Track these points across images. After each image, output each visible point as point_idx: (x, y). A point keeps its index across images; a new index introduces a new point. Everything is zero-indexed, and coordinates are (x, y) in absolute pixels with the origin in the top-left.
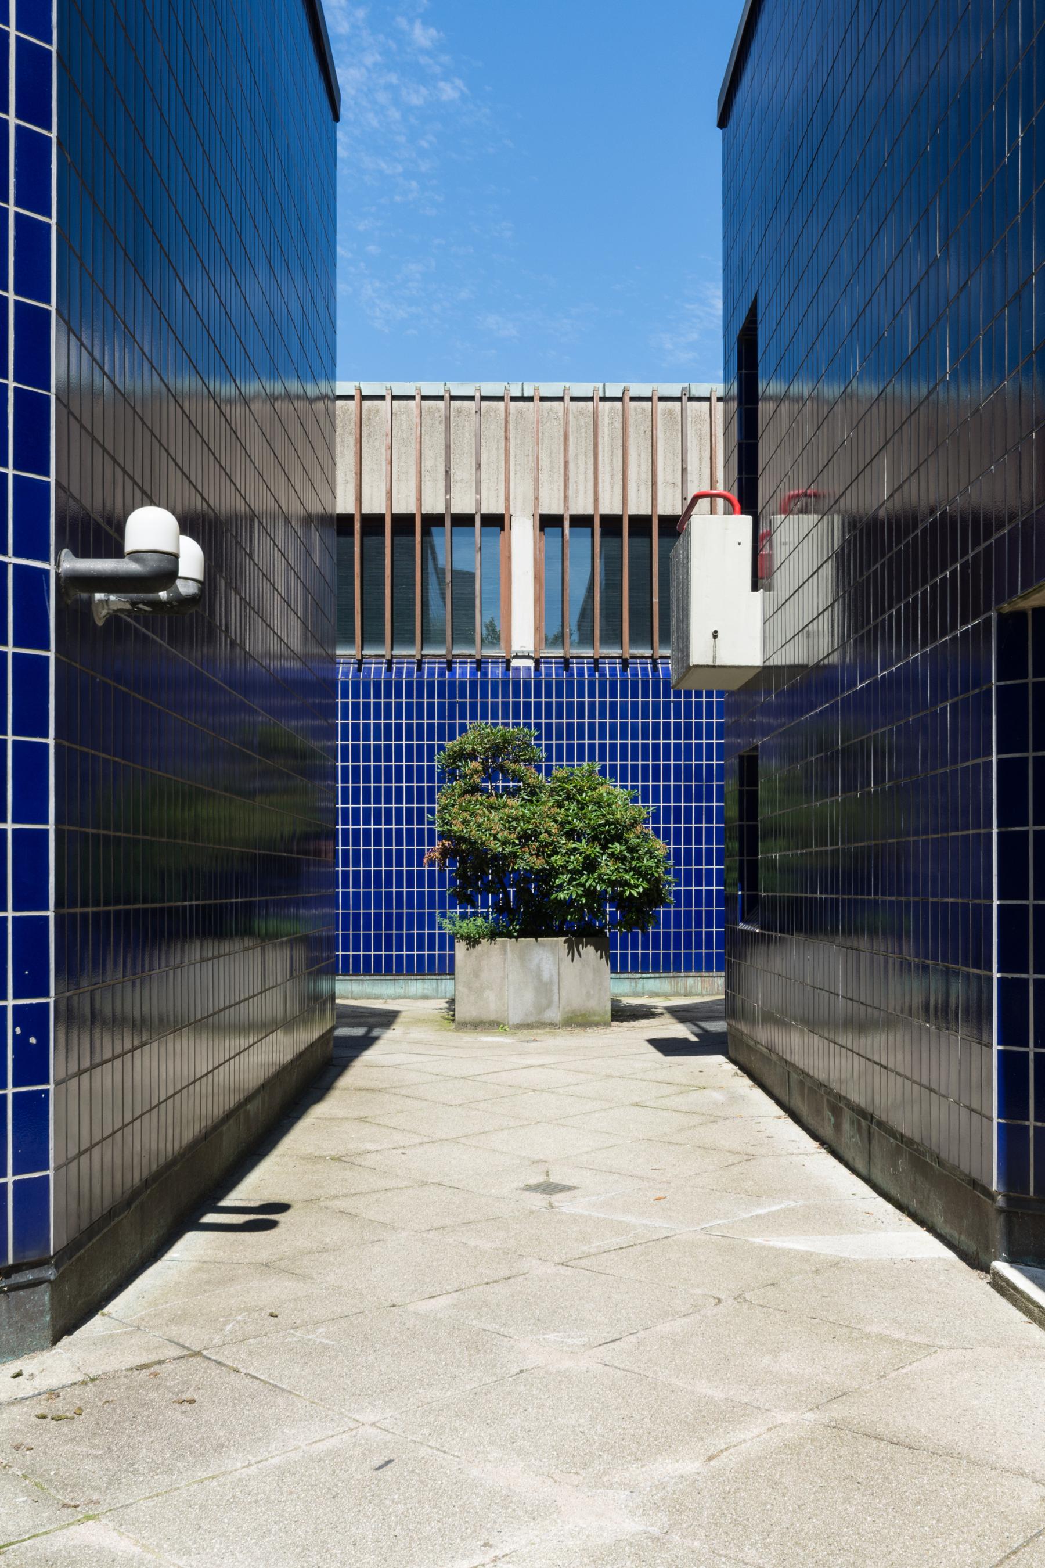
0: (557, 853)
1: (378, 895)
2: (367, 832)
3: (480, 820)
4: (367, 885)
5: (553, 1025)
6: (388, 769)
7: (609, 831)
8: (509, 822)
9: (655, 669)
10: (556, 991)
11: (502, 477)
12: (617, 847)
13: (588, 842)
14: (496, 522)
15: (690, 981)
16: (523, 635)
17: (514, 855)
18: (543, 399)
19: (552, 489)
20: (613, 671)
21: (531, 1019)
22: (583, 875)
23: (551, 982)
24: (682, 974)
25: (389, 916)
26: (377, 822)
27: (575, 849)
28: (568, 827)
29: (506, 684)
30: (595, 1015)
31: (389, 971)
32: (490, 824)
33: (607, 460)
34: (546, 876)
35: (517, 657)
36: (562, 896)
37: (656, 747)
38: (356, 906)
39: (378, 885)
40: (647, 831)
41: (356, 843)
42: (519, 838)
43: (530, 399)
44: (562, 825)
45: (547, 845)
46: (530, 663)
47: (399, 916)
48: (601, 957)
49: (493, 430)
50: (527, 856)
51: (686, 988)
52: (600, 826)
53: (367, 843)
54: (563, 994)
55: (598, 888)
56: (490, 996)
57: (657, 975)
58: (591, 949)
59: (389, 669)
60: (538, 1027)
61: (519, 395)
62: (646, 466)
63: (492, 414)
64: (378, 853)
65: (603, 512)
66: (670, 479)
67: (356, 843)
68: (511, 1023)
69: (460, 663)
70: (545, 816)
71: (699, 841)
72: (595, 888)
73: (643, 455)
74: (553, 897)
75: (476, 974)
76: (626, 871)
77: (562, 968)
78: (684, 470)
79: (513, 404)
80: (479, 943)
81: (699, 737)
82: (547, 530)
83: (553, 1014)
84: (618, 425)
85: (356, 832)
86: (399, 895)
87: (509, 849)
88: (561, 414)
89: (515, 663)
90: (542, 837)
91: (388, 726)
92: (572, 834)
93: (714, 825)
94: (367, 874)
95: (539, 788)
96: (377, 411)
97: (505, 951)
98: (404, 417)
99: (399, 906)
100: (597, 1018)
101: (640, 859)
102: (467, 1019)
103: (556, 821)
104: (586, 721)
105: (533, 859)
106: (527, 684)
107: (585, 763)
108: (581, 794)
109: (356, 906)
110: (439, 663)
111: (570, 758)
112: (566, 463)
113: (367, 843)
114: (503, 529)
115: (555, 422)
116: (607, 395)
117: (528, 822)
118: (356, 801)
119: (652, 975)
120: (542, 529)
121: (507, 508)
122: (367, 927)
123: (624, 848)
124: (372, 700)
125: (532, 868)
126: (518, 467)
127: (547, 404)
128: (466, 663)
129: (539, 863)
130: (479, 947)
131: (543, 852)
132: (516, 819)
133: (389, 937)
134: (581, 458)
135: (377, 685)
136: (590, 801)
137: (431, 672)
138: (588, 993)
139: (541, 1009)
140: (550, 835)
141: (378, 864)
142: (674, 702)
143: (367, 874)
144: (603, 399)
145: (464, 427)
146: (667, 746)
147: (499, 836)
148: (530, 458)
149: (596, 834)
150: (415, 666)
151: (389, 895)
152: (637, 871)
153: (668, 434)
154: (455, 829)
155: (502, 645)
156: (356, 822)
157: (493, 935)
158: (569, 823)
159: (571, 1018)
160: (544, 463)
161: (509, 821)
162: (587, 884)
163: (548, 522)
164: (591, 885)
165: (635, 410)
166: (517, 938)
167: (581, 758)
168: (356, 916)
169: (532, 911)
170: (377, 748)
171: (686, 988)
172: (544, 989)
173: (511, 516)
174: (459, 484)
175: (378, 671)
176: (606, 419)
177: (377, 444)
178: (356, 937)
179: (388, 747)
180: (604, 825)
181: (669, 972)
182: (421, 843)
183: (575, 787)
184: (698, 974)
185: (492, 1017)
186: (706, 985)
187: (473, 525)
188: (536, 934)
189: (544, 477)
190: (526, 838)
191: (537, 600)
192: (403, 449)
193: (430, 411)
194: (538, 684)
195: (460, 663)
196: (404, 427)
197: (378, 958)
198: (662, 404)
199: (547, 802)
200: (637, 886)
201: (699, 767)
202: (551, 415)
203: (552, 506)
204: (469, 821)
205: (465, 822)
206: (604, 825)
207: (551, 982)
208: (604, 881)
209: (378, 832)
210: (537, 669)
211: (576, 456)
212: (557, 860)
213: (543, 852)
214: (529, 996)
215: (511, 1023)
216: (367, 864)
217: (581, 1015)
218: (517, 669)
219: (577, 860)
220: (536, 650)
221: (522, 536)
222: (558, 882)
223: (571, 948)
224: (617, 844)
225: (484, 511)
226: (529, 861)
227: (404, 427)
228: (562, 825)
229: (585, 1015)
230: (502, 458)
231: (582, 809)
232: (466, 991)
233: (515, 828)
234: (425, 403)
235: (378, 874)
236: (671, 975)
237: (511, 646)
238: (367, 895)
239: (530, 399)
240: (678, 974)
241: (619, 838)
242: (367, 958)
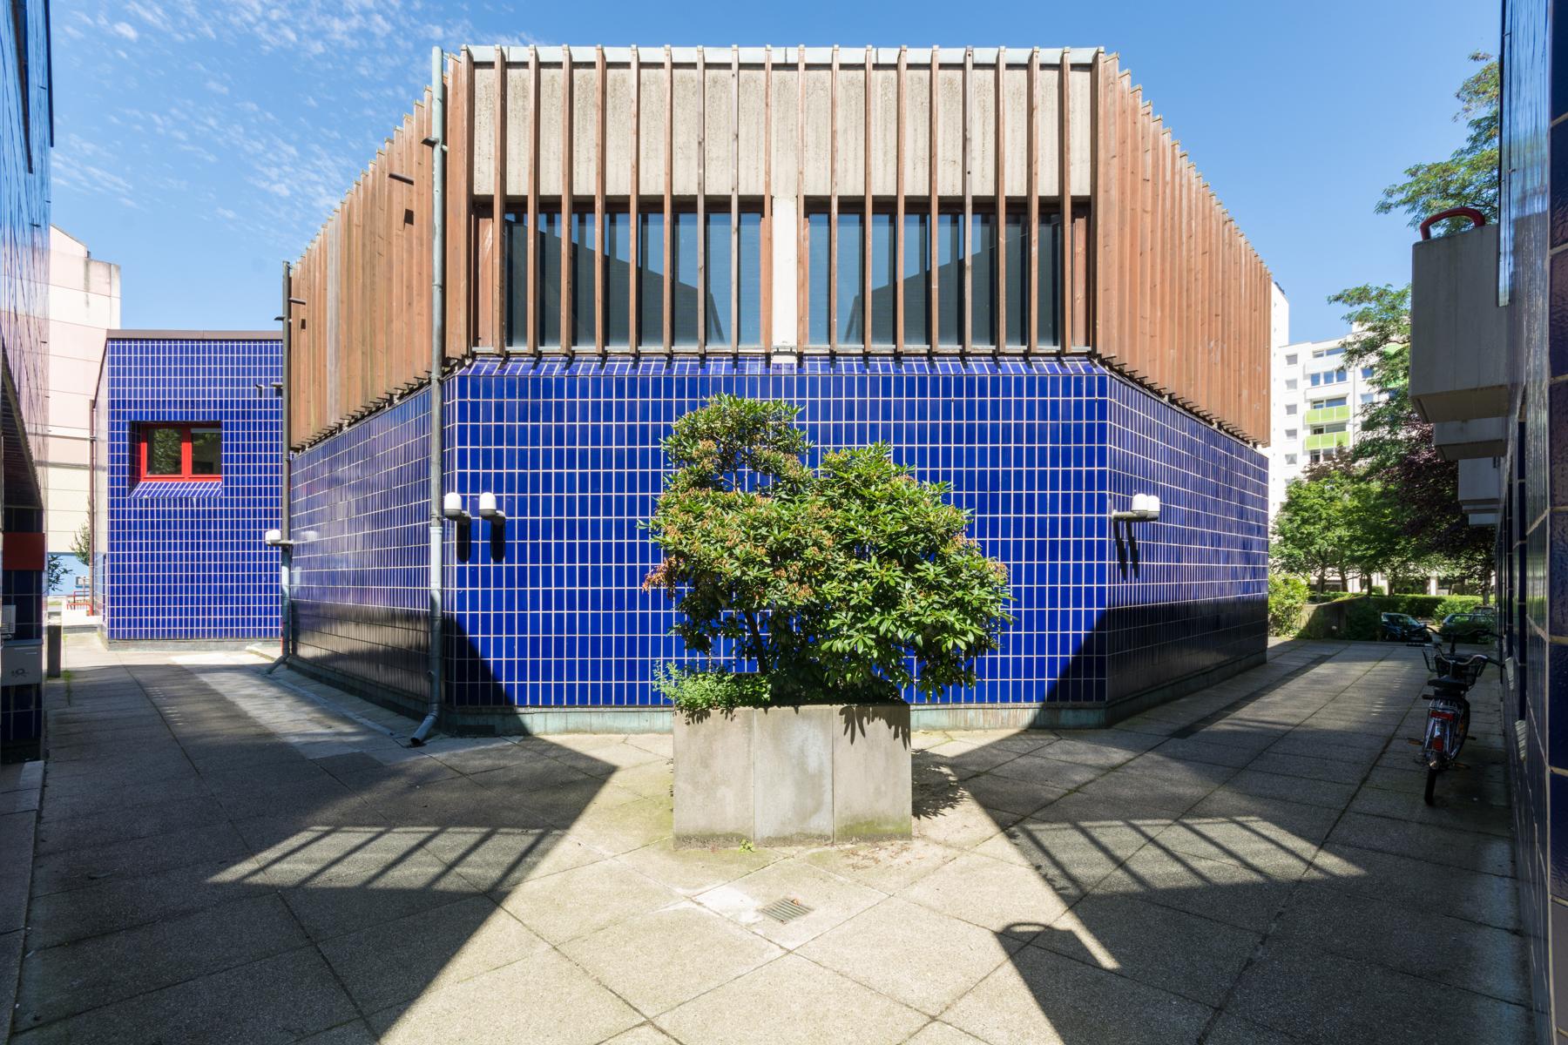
0: (832, 578)
1: (620, 617)
2: (608, 547)
4: (608, 606)
5: (822, 838)
6: (632, 476)
8: (755, 528)
9: (932, 366)
11: (762, 154)
12: (930, 570)
14: (754, 206)
15: (971, 713)
16: (784, 325)
18: (809, 67)
21: (790, 830)
22: (872, 612)
25: (632, 641)
26: (620, 535)
28: (851, 537)
29: (765, 380)
31: (631, 702)
32: (725, 532)
34: (818, 611)
35: (778, 353)
36: (839, 645)
39: (620, 606)
41: (595, 559)
42: (772, 553)
43: (794, 67)
44: (841, 534)
46: (793, 360)
47: (644, 641)
48: (896, 736)
49: (753, 102)
50: (783, 583)
53: (608, 559)
54: (839, 791)
56: (728, 795)
58: (881, 724)
59: (635, 366)
60: (800, 842)
64: (620, 570)
67: (595, 559)
68: (758, 836)
71: (595, 536)
72: (894, 635)
73: (920, 130)
75: (705, 763)
79: (775, 73)
80: (708, 714)
81: (983, 440)
83: (823, 822)
85: (596, 547)
86: (644, 617)
87: (753, 573)
89: (775, 360)
91: (632, 429)
92: (856, 549)
94: (608, 594)
95: (803, 484)
96: (624, 81)
97: (750, 727)
99: (644, 630)
100: (890, 828)
102: (691, 832)
103: (829, 528)
106: (789, 381)
107: (868, 445)
108: (868, 487)
109: (596, 630)
112: (833, 133)
113: (608, 559)
116: (881, 61)
118: (595, 512)
120: (806, 215)
121: (768, 185)
123: (939, 569)
125: (791, 604)
129: (803, 595)
130: (707, 722)
131: (810, 578)
132: (768, 524)
133: (632, 664)
135: (620, 383)
136: (881, 498)
137: (682, 368)
139: (804, 815)
140: (821, 549)
141: (620, 582)
143: (608, 594)
144: (877, 66)
146: (947, 451)
147: (737, 551)
151: (632, 617)
154: (668, 539)
156: (595, 536)
157: (730, 703)
158: (852, 531)
159: (851, 827)
160: (810, 138)
161: (756, 529)
162: (882, 629)
163: (815, 206)
164: (888, 630)
166: (766, 705)
168: (596, 641)
169: (789, 665)
170: (620, 453)
172: (809, 783)
177: (623, 117)
179: (632, 452)
180: (907, 534)
183: (858, 476)
185: (730, 827)
186: (989, 717)
190: (781, 555)
191: (800, 287)
192: (652, 123)
193: (683, 81)
194: (801, 381)
197: (620, 688)
200: (964, 633)
201: (982, 474)
203: (819, 189)
205: (685, 529)
206: (907, 534)
208: (909, 625)
209: (620, 547)
210: (800, 365)
211: (845, 131)
212: (832, 589)
213: (810, 578)
214: (786, 795)
215: (758, 836)
216: (608, 583)
218: (778, 367)
219: (864, 589)
221: (785, 222)
222: (833, 623)
223: (849, 721)
224: (928, 564)
226: (788, 592)
230: (763, 133)
231: (871, 508)
233: (764, 538)
235: (620, 594)
239: (794, 67)
241: (932, 554)
242: (607, 688)
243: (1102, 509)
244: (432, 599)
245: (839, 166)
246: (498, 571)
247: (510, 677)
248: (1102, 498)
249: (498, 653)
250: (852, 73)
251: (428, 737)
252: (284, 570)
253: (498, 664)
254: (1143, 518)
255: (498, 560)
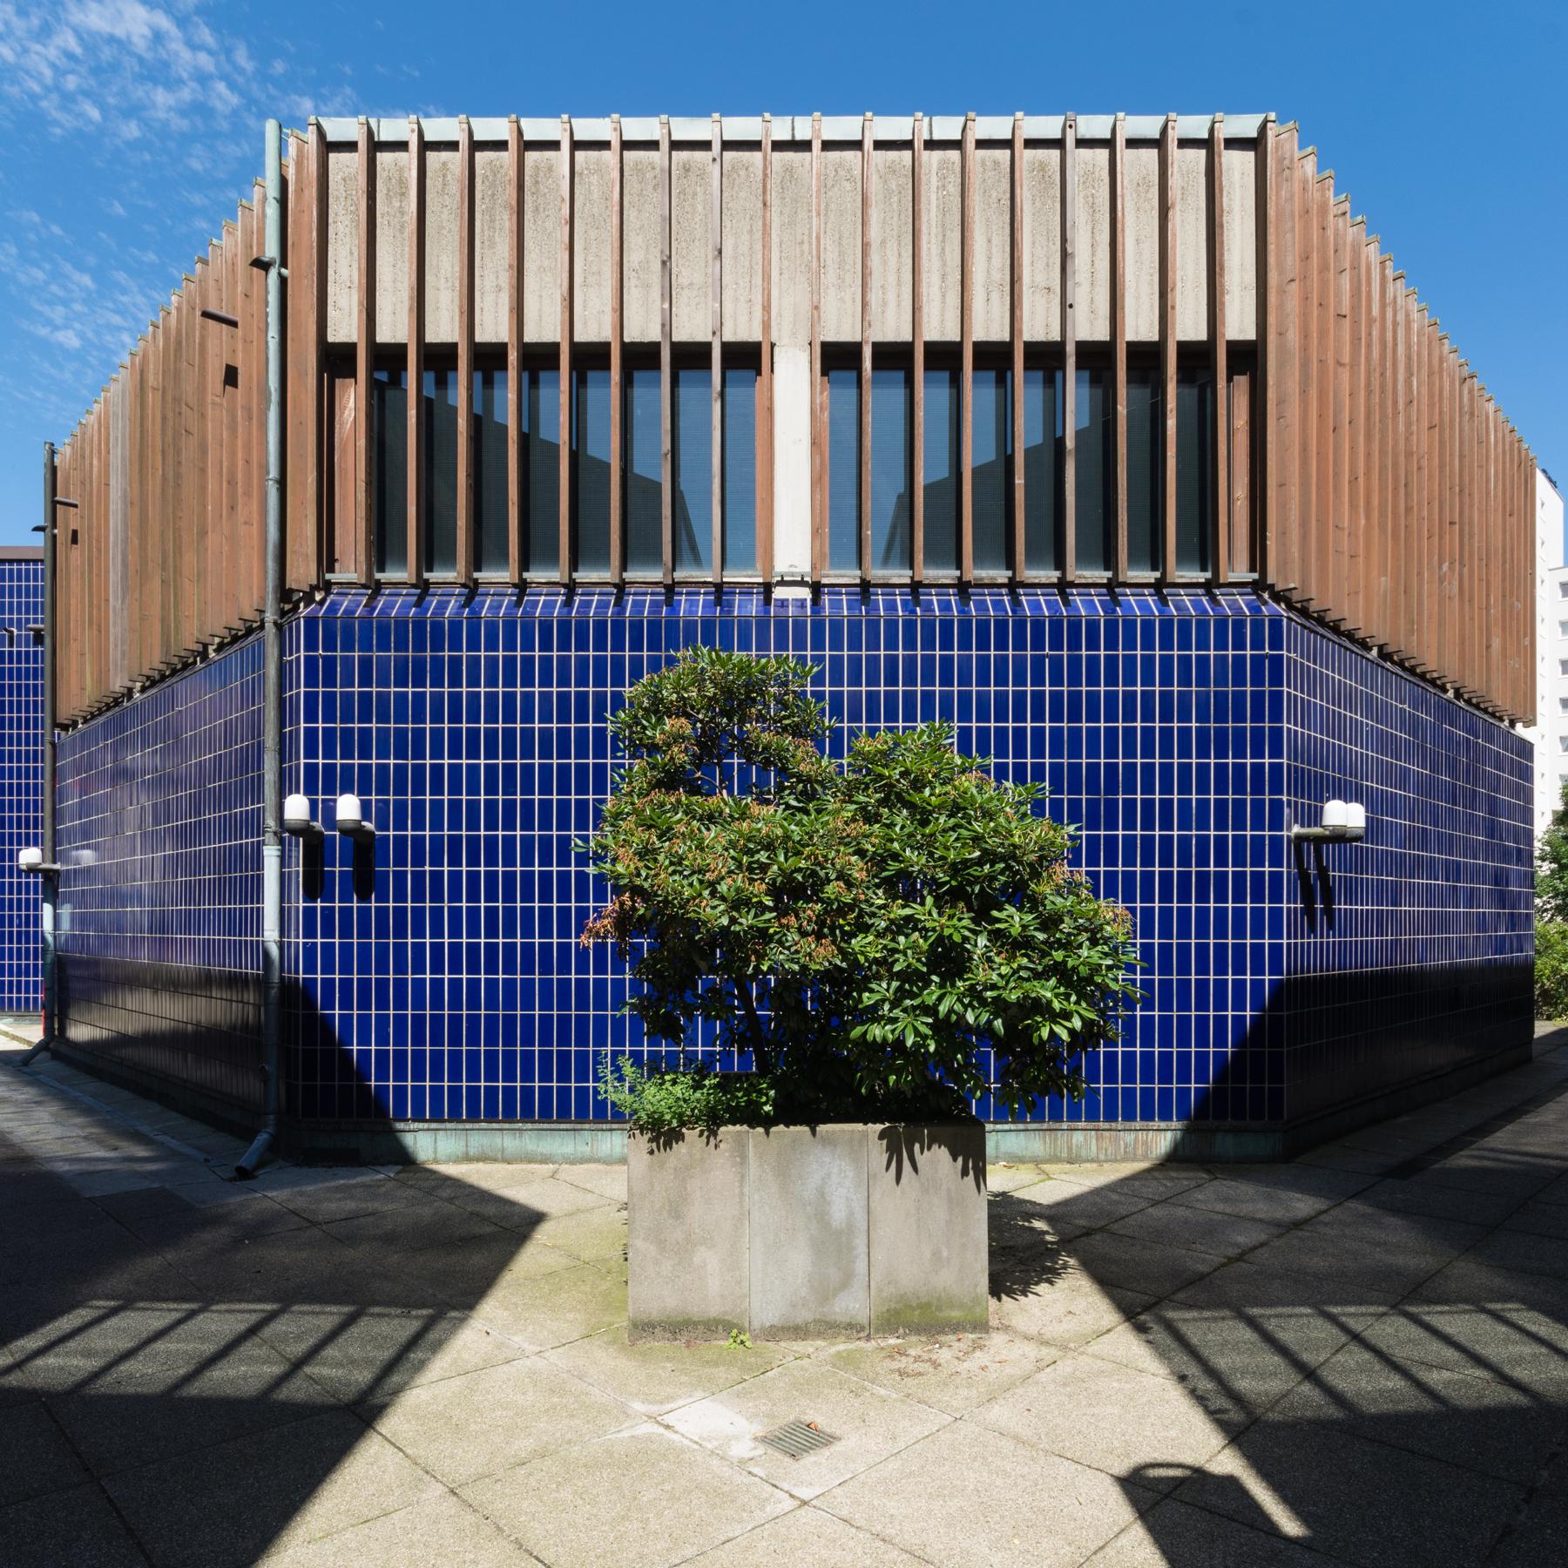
0: (866, 929)
3: (681, 849)
5: (853, 1329)
7: (992, 878)
8: (751, 853)
9: (1016, 603)
10: (862, 1249)
11: (758, 280)
12: (1014, 919)
13: (938, 905)
14: (746, 359)
15: (1078, 1137)
16: (793, 542)
17: (763, 935)
19: (842, 300)
20: (945, 606)
21: (804, 1316)
22: (928, 983)
23: (850, 1228)
24: (1065, 1125)
27: (908, 919)
28: (894, 866)
29: (763, 624)
30: (952, 1306)
31: (564, 1115)
32: (707, 857)
33: (935, 250)
35: (782, 583)
36: (876, 1032)
37: (1020, 733)
38: (510, 1004)
40: (1077, 877)
41: (509, 896)
42: (775, 891)
43: (805, 146)
44: (878, 861)
45: (844, 909)
46: (805, 593)
48: (965, 1173)
50: (792, 936)
51: (1070, 1149)
52: (966, 863)
54: (879, 1256)
55: (970, 1017)
56: (709, 1260)
57: (1021, 1126)
58: (941, 1153)
60: (819, 1335)
61: (788, 137)
62: (1001, 259)
63: (742, 173)
65: (927, 338)
66: (1041, 279)
68: (756, 1324)
69: (688, 594)
70: (836, 835)
72: (962, 1017)
74: (857, 1032)
76: (1037, 976)
77: (876, 1196)
78: (1065, 255)
79: (777, 155)
80: (680, 1137)
82: (833, 374)
83: (853, 1304)
84: (954, 189)
87: (747, 920)
88: (857, 172)
89: (779, 593)
90: (832, 889)
92: (902, 886)
93: (1120, 869)
95: (821, 783)
96: (550, 169)
98: (594, 179)
100: (955, 1314)
101: (1068, 946)
102: (655, 1315)
103: (861, 853)
104: (901, 688)
105: (809, 944)
106: (799, 626)
108: (920, 790)
110: (653, 594)
111: (891, 716)
112: (865, 247)
114: (759, 373)
115: (848, 186)
116: (936, 137)
117: (798, 853)
119: (1013, 1127)
120: (824, 373)
121: (766, 326)
122: (527, 1040)
124: (537, 654)
125: (804, 968)
126: (786, 263)
127: (834, 155)
128: (698, 594)
129: (823, 955)
130: (680, 1149)
131: (832, 929)
132: (769, 846)
134: (892, 246)
135: (546, 627)
136: (940, 807)
137: (638, 605)
138: (936, 1254)
139: (825, 1293)
140: (850, 885)
142: (1051, 657)
144: (931, 145)
145: (695, 194)
148: (806, 247)
149: (961, 887)
150: (613, 599)
152: (1062, 973)
153: (1038, 204)
155: (759, 566)
157: (713, 1120)
158: (896, 857)
159: (897, 1312)
160: (830, 256)
162: (943, 1009)
163: (837, 359)
164: (951, 1011)
165: (983, 163)
167: (910, 716)
171: (1070, 1149)
172: (833, 1244)
173: (773, 346)
174: (686, 291)
175: (549, 606)
176: (934, 179)
177: (549, 224)
178: (510, 1057)
180: (980, 862)
181: (1042, 1120)
182: (582, 896)
183: (902, 774)
184: (1091, 1125)
185: (714, 1310)
187: (708, 366)
188: (812, 1118)
189: (830, 277)
190: (789, 893)
191: (816, 482)
192: (593, 234)
193: (639, 169)
194: (818, 626)
195: (688, 594)
196: (595, 196)
198: (1030, 154)
199: (838, 815)
200: (1067, 1015)
202: (842, 173)
203: (843, 330)
204: (655, 851)
205: (646, 853)
206: (980, 862)
207: (850, 1228)
208: (983, 1002)
210: (816, 601)
211: (883, 242)
213: (832, 929)
214: (799, 1261)
215: (756, 1324)
217: (920, 1306)
219: (915, 946)
220: (813, 567)
221: (793, 385)
223: (894, 1151)
224: (1011, 910)
225: (729, 337)
226: (800, 950)
227: (595, 196)
228: (878, 861)
229: (929, 1305)
231: (924, 823)
232: (652, 1249)
233: (764, 868)
234: (630, 155)
236: (1045, 1126)
237: (772, 567)
238: (528, 985)
239: (805, 146)
240: (1057, 1126)
241: (1018, 893)
243: (1277, 824)
244: (267, 954)
245: (873, 298)
246: (363, 913)
247: (382, 1075)
248: (1277, 807)
249: (364, 1040)
250: (892, 155)
251: (261, 1164)
252: (47, 909)
253: (364, 1055)
254: (1340, 837)
255: (364, 897)
